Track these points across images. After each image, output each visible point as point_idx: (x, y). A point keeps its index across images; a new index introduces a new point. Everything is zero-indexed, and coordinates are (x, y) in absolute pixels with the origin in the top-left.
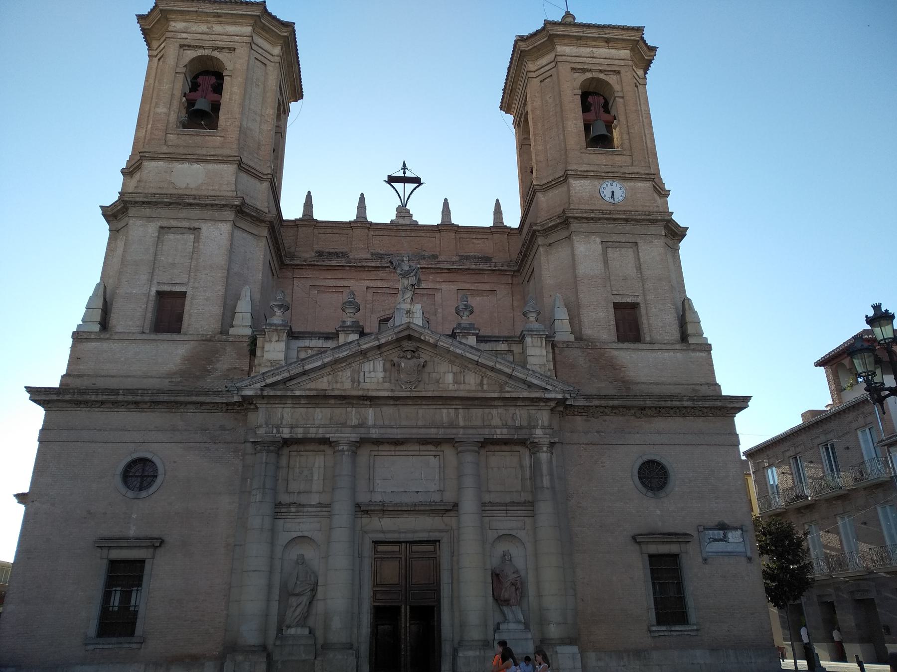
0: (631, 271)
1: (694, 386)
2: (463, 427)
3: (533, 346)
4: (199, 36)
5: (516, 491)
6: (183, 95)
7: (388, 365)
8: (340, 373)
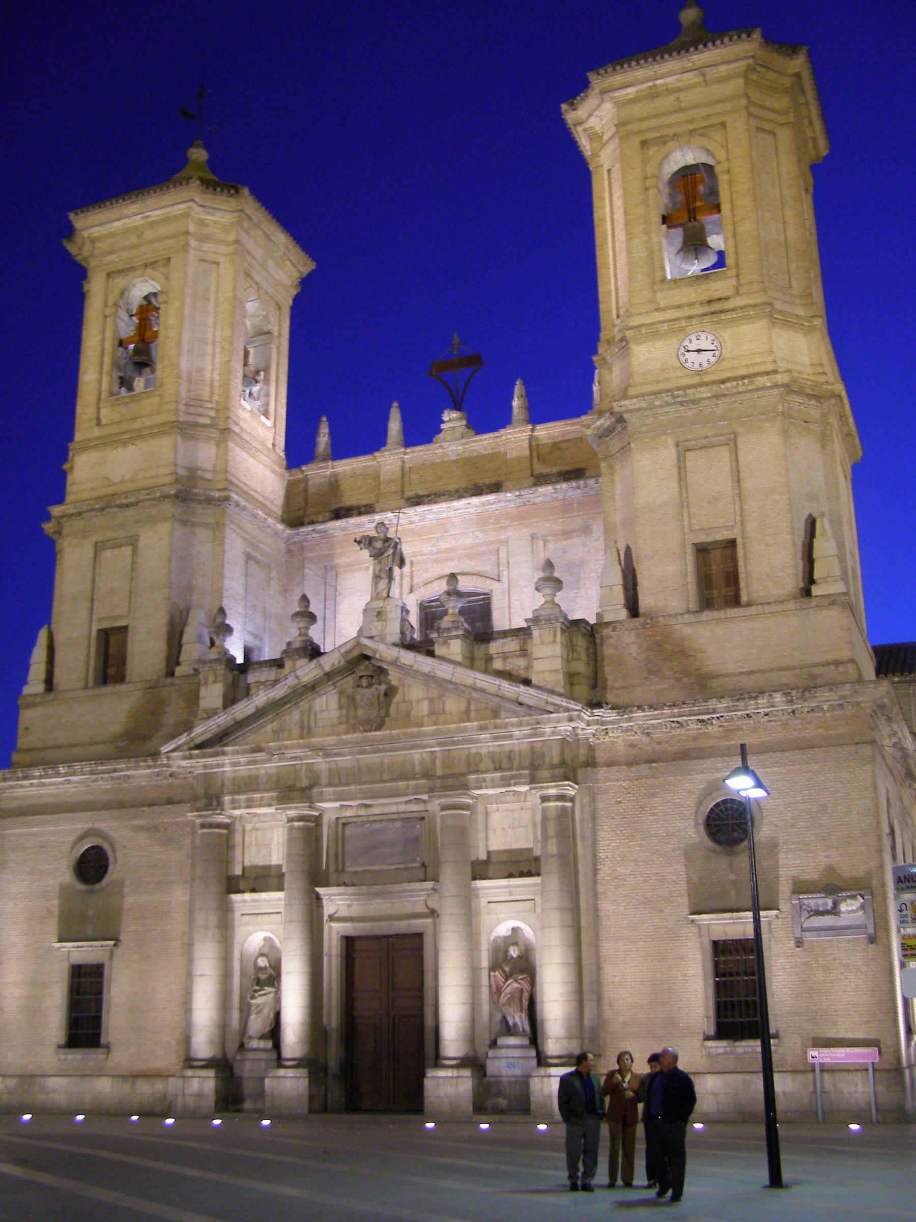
0: (725, 485)
1: (811, 669)
3: (543, 643)
4: (125, 254)
5: (526, 861)
6: (117, 343)
7: (344, 701)
8: (287, 717)
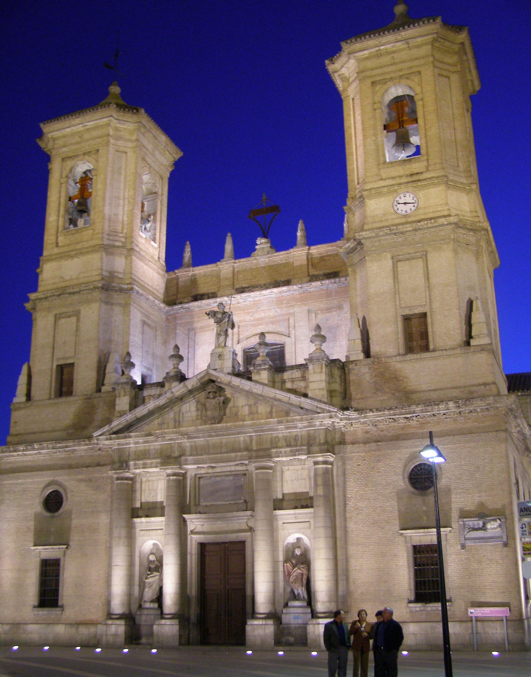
1: (470, 388)
2: (256, 451)
3: (315, 373)
6: (68, 199)
7: (200, 406)
8: (167, 416)
